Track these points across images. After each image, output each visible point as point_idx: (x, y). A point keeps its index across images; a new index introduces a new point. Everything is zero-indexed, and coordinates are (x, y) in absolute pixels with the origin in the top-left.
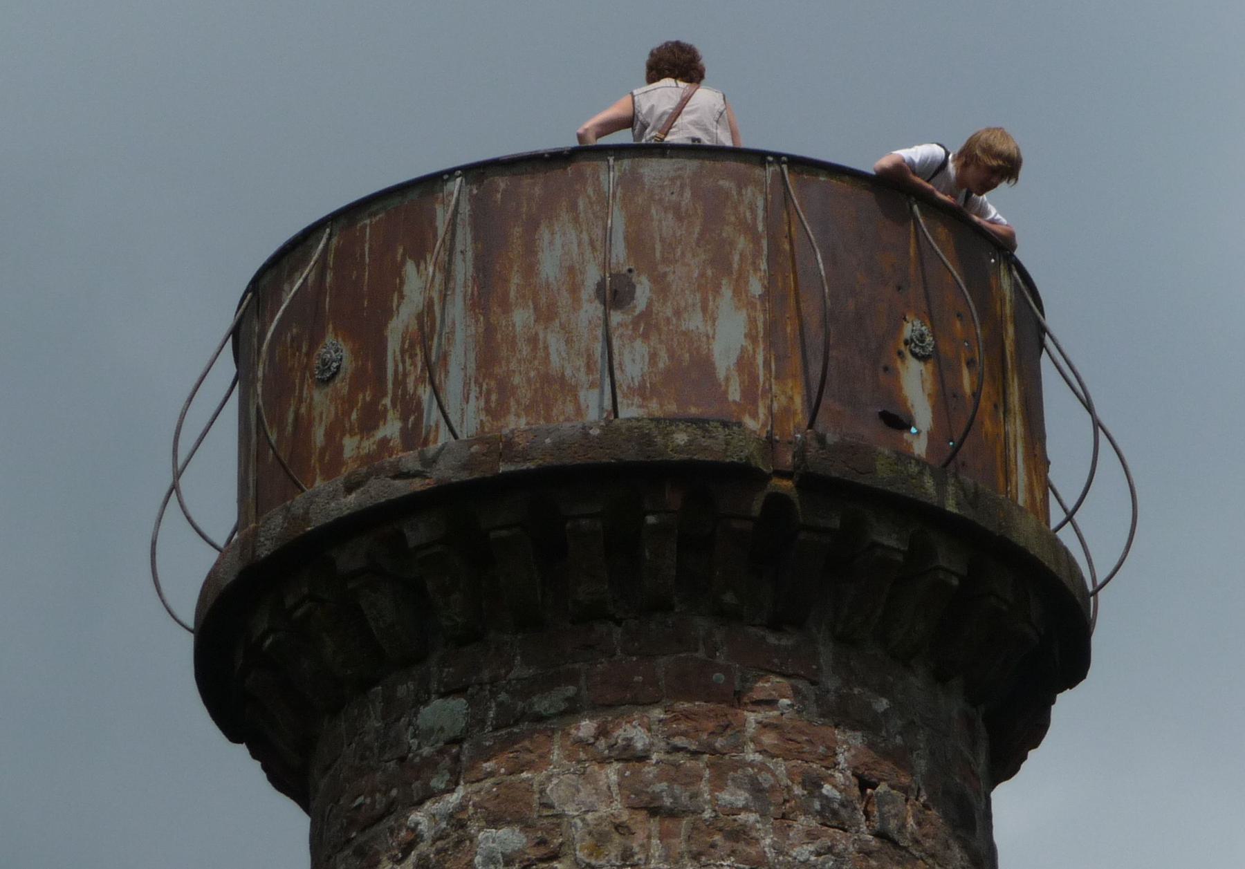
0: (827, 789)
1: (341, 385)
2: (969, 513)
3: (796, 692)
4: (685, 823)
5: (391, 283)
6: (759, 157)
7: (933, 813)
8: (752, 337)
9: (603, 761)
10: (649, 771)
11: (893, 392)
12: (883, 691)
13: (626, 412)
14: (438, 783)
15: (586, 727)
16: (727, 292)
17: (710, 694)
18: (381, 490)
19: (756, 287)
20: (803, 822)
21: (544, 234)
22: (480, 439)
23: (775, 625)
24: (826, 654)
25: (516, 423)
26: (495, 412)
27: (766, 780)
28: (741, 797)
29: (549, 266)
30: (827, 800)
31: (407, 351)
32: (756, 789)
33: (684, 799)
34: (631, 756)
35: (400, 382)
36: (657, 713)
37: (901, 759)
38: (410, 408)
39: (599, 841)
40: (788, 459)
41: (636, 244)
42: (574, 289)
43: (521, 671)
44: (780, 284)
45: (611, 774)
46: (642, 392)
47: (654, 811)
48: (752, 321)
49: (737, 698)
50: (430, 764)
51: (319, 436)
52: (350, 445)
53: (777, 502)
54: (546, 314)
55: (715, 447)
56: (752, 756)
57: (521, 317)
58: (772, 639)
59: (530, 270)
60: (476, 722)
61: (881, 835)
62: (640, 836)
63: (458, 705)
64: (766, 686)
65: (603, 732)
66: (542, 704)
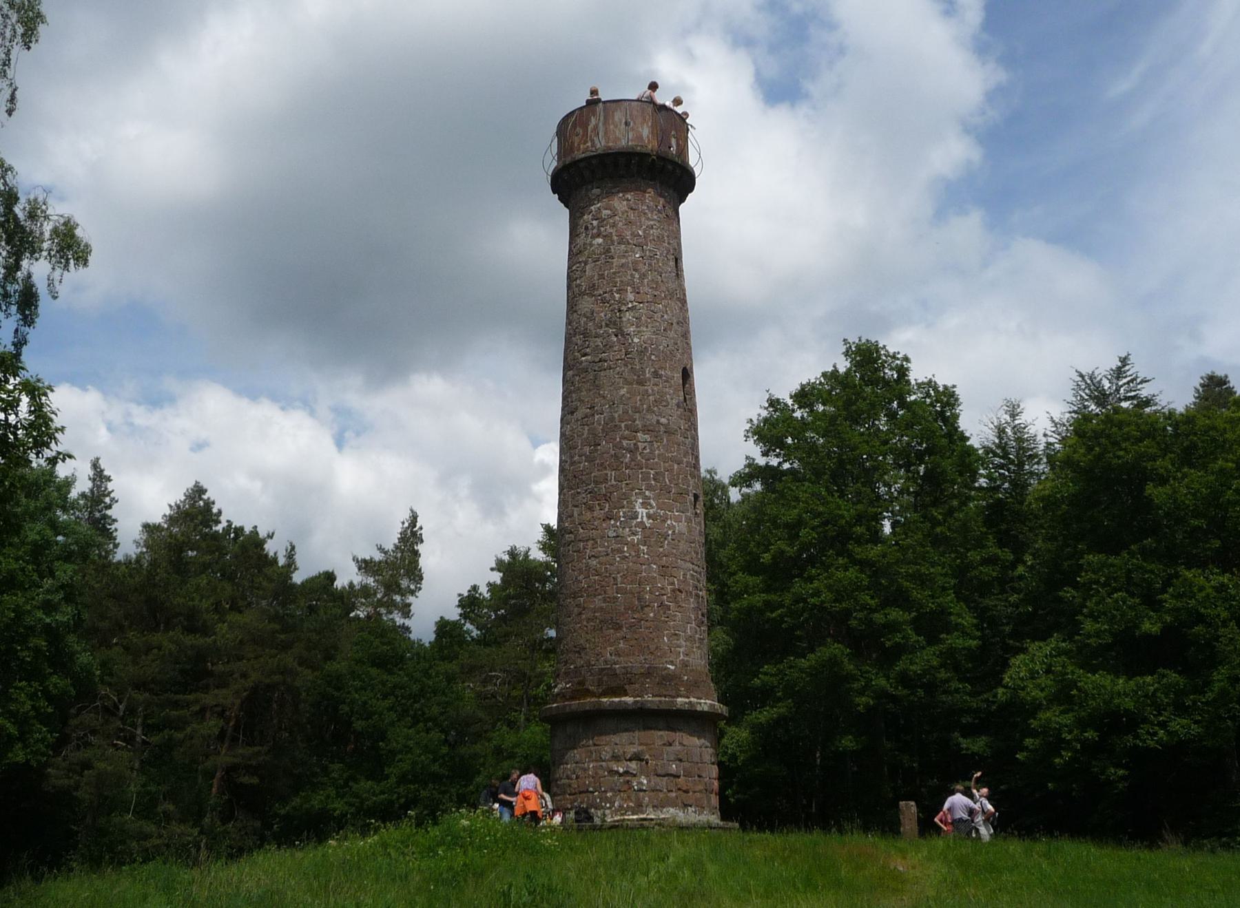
1: (580, 136)
5: (588, 120)
11: (670, 144)
13: (630, 143)
14: (596, 202)
15: (621, 195)
18: (588, 154)
20: (655, 212)
22: (605, 146)
23: (651, 180)
25: (610, 144)
26: (607, 142)
29: (616, 118)
31: (592, 132)
34: (628, 200)
35: (591, 136)
37: (669, 203)
38: (592, 141)
40: (655, 153)
42: (621, 123)
44: (1011, 642)
45: (625, 202)
46: (632, 140)
47: (632, 209)
49: (645, 192)
50: (594, 199)
51: (576, 145)
52: (582, 147)
53: (653, 160)
54: (616, 127)
55: (644, 150)
57: (612, 127)
59: (613, 119)
60: (602, 193)
63: (599, 190)
64: (649, 190)
66: (613, 191)
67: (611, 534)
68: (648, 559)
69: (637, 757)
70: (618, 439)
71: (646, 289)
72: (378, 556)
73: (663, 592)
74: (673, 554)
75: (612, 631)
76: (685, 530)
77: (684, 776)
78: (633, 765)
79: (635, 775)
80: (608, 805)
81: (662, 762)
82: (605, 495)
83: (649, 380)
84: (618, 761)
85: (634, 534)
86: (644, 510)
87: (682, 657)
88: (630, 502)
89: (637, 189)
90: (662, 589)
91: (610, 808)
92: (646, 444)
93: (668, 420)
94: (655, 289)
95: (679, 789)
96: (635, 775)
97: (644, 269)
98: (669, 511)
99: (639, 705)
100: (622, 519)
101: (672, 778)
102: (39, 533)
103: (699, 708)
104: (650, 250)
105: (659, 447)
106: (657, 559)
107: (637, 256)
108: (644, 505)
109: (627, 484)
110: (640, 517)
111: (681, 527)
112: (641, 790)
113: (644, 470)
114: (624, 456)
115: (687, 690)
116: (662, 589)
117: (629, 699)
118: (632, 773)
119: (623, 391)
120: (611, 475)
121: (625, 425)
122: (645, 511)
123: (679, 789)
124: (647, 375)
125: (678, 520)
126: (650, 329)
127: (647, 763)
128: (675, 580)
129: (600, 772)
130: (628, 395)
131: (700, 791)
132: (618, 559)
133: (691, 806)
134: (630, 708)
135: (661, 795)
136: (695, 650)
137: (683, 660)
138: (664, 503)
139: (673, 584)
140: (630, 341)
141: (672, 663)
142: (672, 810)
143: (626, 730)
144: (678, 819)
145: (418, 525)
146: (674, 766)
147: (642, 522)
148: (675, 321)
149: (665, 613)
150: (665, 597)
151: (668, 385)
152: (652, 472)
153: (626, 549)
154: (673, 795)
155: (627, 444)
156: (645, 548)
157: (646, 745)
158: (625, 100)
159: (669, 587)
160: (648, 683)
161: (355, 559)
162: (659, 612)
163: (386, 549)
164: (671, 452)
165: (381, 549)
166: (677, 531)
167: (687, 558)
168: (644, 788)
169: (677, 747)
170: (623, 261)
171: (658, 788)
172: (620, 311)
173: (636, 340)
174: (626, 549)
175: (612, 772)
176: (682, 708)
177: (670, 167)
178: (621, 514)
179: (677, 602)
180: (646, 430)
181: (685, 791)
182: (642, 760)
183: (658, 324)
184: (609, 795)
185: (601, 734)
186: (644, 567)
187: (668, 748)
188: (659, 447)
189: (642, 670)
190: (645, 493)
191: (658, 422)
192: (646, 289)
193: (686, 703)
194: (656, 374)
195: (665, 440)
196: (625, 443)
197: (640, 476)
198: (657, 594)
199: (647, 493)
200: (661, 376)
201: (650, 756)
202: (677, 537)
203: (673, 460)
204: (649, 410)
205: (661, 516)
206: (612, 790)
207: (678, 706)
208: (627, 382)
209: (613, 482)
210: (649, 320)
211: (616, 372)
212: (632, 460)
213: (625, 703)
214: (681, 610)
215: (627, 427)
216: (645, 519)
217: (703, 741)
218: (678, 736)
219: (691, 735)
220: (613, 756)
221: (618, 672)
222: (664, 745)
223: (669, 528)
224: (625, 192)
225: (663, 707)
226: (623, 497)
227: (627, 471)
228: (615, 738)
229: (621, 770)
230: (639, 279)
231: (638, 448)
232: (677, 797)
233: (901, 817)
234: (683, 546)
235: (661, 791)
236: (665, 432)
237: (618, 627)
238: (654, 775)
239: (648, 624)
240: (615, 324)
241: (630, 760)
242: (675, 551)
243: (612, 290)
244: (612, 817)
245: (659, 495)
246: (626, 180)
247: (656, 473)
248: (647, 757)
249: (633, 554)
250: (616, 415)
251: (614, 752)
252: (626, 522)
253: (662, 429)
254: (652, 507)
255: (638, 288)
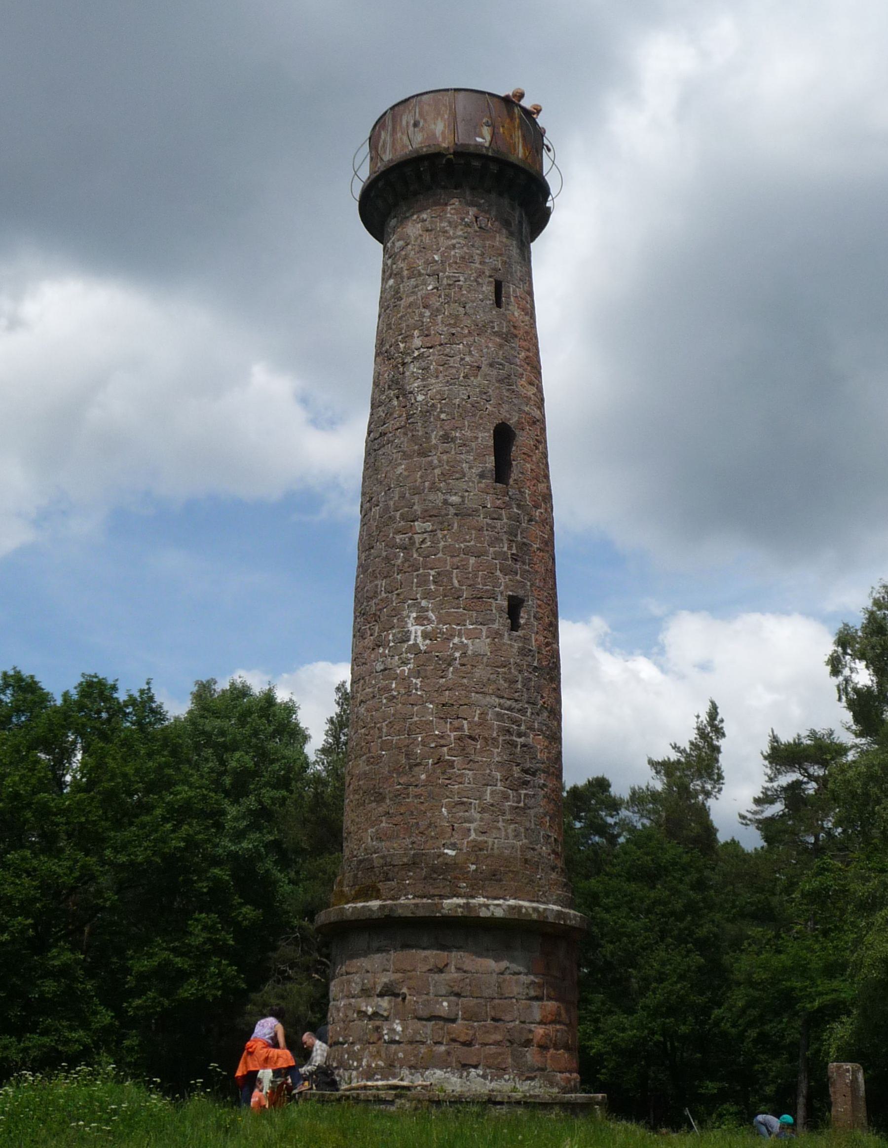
0: (466, 220)
2: (495, 155)
3: (460, 201)
4: (433, 232)
6: (447, 90)
7: (496, 223)
8: (445, 127)
9: (418, 223)
10: (427, 223)
12: (483, 198)
15: (415, 217)
16: (439, 119)
17: (440, 204)
19: (446, 116)
20: (460, 227)
21: (403, 117)
23: (456, 188)
24: (468, 193)
27: (451, 220)
28: (446, 224)
30: (466, 222)
32: (450, 222)
33: (434, 227)
34: (424, 221)
36: (429, 211)
37: (486, 212)
39: (416, 238)
41: (421, 114)
43: (405, 209)
47: (427, 231)
48: (445, 124)
49: (446, 204)
56: (449, 215)
57: (399, 135)
58: (455, 191)
60: (398, 222)
61: (480, 228)
62: (424, 236)
64: (452, 201)
65: (418, 217)
66: (408, 215)
67: (380, 667)
68: (421, 696)
69: (388, 991)
70: (391, 535)
71: (441, 328)
72: (674, 756)
73: (442, 742)
74: (462, 685)
75: (374, 805)
76: (486, 650)
77: (464, 1019)
78: (385, 1003)
79: (387, 1019)
80: (355, 1064)
81: (425, 997)
82: (375, 614)
83: (436, 447)
84: (369, 996)
85: (404, 663)
86: (418, 627)
87: (473, 836)
88: (402, 620)
89: (436, 203)
90: (442, 737)
91: (357, 1069)
92: (425, 535)
93: (462, 497)
94: (454, 326)
95: (454, 1040)
96: (387, 1019)
97: (435, 302)
98: (458, 624)
99: (386, 912)
100: (392, 644)
101: (441, 1023)
102: (238, 761)
103: (484, 913)
104: (448, 277)
105: (445, 536)
106: (435, 694)
107: (430, 288)
108: (419, 621)
109: (398, 594)
110: (412, 637)
111: (482, 645)
112: (392, 1042)
113: (421, 571)
114: (396, 557)
115: (472, 886)
116: (442, 737)
117: (375, 904)
118: (382, 1016)
119: (400, 470)
120: (381, 585)
121: (401, 515)
122: (420, 629)
123: (454, 1040)
124: (434, 442)
125: (474, 636)
126: (441, 378)
127: (404, 999)
128: (465, 722)
129: (350, 1013)
130: (406, 473)
131: (497, 1043)
132: (384, 701)
133: (476, 1067)
134: (375, 916)
135: (423, 1049)
136: (500, 824)
137: (474, 841)
138: (449, 614)
139: (460, 728)
140: (413, 401)
141: (453, 846)
142: (439, 1073)
143: (379, 950)
144: (449, 1089)
145: (719, 718)
146: (445, 1004)
147: (416, 645)
148: (484, 363)
149: (443, 773)
150: (445, 749)
151: (464, 449)
152: (432, 572)
153: (394, 686)
154: (443, 1048)
155: (401, 540)
156: (418, 681)
157: (404, 971)
158: (413, 97)
159: (452, 735)
160: (410, 878)
161: (651, 763)
162: (434, 771)
163: (682, 748)
164: (465, 541)
165: (675, 747)
166: (470, 652)
167: (490, 689)
168: (397, 1038)
169: (452, 974)
170: (411, 299)
171: (418, 1038)
172: (404, 364)
173: (420, 398)
174: (394, 686)
175: (362, 1014)
176: (452, 914)
177: (476, 163)
178: (391, 637)
179: (466, 756)
180: (428, 516)
181: (464, 1044)
182: (397, 995)
183: (454, 371)
184: (357, 1047)
185: (351, 957)
186: (416, 708)
187: (436, 976)
188: (445, 536)
189: (405, 860)
190: (420, 603)
191: (445, 502)
192: (441, 328)
193: (459, 906)
194: (446, 438)
195: (456, 525)
196: (398, 538)
197: (415, 580)
198: (433, 745)
199: (424, 603)
200: (453, 440)
201: (409, 988)
202: (470, 661)
203: (467, 552)
204: (434, 488)
205: (444, 633)
206: (360, 1040)
207: (445, 912)
208: (406, 456)
209: (384, 595)
210: (441, 368)
211: (394, 445)
212: (406, 560)
213: (370, 909)
214: (476, 766)
215: (402, 517)
216: (420, 640)
217: (505, 964)
218: (455, 957)
219: (480, 955)
220: (363, 990)
221: (376, 864)
222: (430, 970)
223: (456, 648)
224: (420, 211)
225: (421, 913)
226: (393, 613)
227: (399, 577)
228: (364, 963)
229: (370, 1010)
230: (430, 317)
231: (414, 543)
232: (448, 1053)
233: (831, 1090)
234: (481, 673)
235: (423, 1043)
236: (456, 514)
237: (380, 798)
238: (413, 1018)
239: (418, 790)
240: (397, 383)
241: (381, 995)
242: (465, 681)
243: (397, 341)
244: (358, 1082)
245: (442, 603)
246: (421, 197)
247: (438, 573)
248: (405, 990)
249: (403, 691)
250: (392, 503)
251: (363, 984)
252: (395, 647)
253: (452, 511)
254: (430, 621)
255: (428, 329)
